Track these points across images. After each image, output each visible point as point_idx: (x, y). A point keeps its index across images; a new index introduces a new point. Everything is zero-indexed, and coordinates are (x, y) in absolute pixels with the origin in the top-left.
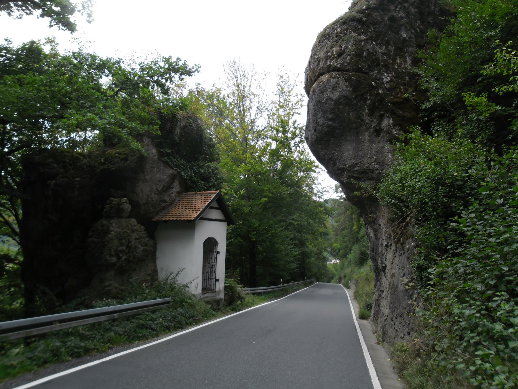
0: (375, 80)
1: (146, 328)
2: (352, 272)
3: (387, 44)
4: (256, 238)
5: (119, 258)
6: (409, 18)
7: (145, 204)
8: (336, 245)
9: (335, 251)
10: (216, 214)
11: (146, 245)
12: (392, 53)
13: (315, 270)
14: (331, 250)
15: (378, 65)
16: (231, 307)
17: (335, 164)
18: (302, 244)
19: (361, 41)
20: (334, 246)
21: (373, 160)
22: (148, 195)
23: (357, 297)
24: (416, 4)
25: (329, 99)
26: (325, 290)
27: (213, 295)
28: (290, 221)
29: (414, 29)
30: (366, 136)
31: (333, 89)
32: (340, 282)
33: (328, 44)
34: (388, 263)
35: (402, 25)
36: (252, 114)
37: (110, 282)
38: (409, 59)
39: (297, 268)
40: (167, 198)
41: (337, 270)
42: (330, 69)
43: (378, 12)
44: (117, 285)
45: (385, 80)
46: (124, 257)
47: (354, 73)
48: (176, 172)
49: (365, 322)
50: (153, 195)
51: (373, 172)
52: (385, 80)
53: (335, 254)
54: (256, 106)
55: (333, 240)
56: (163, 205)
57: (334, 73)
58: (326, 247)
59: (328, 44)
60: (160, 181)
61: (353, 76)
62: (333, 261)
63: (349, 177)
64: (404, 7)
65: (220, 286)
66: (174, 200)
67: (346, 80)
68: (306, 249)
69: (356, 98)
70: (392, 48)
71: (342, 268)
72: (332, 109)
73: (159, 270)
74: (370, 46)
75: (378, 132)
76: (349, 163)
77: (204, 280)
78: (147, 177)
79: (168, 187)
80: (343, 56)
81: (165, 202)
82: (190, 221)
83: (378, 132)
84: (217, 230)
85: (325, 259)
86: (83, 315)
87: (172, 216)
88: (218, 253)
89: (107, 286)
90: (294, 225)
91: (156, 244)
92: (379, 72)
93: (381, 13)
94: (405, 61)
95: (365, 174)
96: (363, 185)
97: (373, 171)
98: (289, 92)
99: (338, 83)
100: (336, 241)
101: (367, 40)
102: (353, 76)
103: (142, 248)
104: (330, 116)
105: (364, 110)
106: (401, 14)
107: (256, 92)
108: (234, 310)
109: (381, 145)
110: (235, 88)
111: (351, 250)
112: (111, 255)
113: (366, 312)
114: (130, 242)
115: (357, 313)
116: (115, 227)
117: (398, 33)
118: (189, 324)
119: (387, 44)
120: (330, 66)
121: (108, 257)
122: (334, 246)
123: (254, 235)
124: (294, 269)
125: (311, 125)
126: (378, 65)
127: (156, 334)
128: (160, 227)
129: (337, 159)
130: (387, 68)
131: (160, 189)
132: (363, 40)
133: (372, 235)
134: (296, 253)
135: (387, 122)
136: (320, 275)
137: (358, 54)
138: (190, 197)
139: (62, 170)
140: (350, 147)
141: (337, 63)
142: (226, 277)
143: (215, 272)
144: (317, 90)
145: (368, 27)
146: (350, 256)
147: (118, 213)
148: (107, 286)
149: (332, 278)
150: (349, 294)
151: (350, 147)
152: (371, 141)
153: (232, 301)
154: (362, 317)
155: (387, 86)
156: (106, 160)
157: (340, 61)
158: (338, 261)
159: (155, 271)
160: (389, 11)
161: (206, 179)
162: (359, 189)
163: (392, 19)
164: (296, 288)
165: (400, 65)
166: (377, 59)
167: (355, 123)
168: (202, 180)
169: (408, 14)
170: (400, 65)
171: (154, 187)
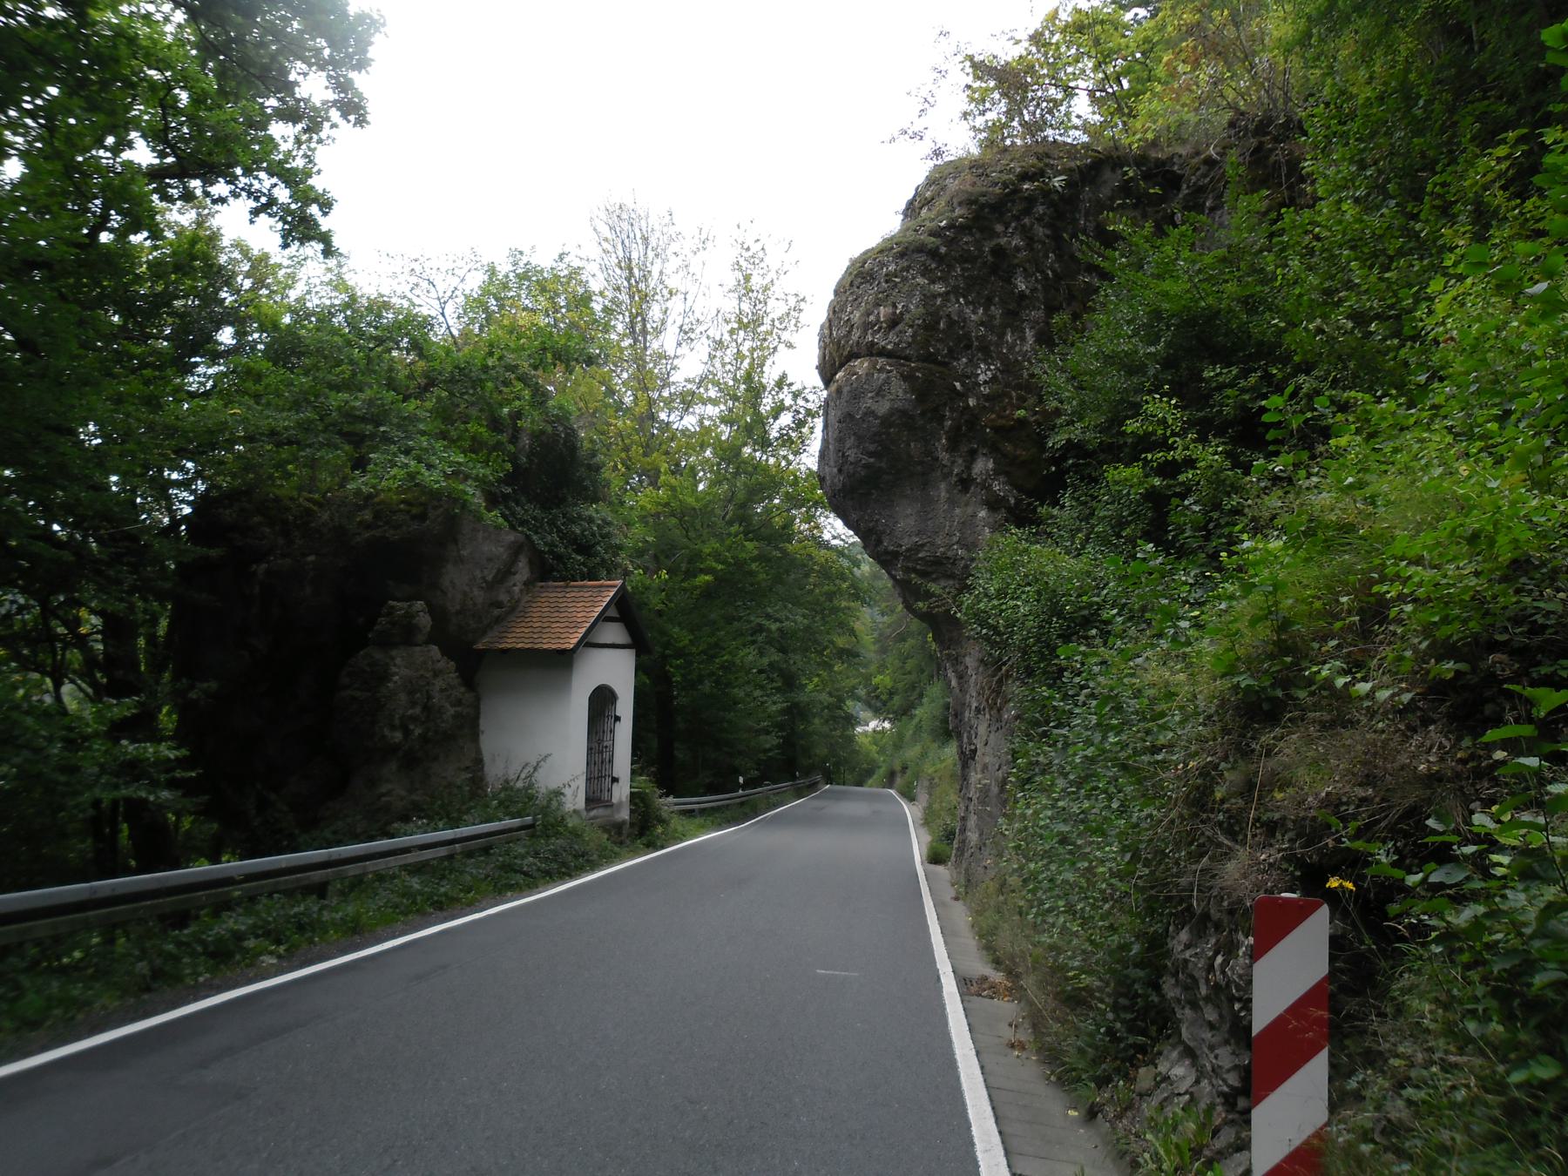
0: (962, 378)
1: (516, 872)
2: (924, 755)
3: (988, 302)
4: (683, 676)
5: (407, 733)
6: (1032, 249)
7: (458, 613)
8: (883, 680)
9: (877, 697)
10: (614, 633)
11: (459, 703)
12: (997, 322)
13: (821, 751)
14: (868, 694)
15: (969, 347)
16: (644, 840)
17: (879, 542)
18: (790, 682)
19: (935, 296)
20: (875, 681)
21: (955, 539)
22: (465, 594)
23: (927, 821)
24: (1047, 219)
25: (870, 413)
26: (853, 804)
27: (607, 812)
28: (758, 620)
29: (1043, 272)
30: (942, 491)
31: (877, 394)
32: (890, 785)
33: (870, 293)
34: (979, 743)
35: (1018, 265)
36: (668, 341)
37: (389, 786)
38: (1029, 334)
39: (778, 746)
40: (504, 597)
41: (882, 751)
42: (872, 351)
43: (972, 235)
44: (403, 793)
45: (982, 378)
46: (418, 731)
47: (920, 364)
48: (521, 538)
49: (940, 868)
50: (476, 592)
51: (954, 564)
52: (982, 378)
53: (879, 706)
54: (679, 323)
55: (873, 668)
56: (496, 612)
57: (881, 361)
58: (854, 688)
59: (870, 293)
60: (490, 560)
61: (918, 369)
62: (873, 724)
63: (907, 570)
64: (1024, 226)
65: (621, 792)
66: (518, 601)
67: (905, 378)
68: (802, 698)
69: (923, 414)
70: (996, 311)
71: (899, 743)
72: (875, 434)
73: (486, 758)
74: (953, 308)
75: (965, 483)
76: (907, 543)
77: (588, 780)
78: (464, 553)
79: (506, 573)
80: (899, 327)
81: (499, 605)
82: (563, 652)
83: (965, 483)
84: (615, 669)
85: (851, 721)
86: (344, 856)
87: (518, 638)
88: (618, 719)
89: (384, 795)
90: (769, 630)
91: (478, 699)
92: (970, 361)
93: (978, 236)
94: (1023, 339)
95: (939, 566)
96: (934, 587)
97: (955, 560)
98: (766, 289)
99: (887, 381)
100: (882, 668)
101: (947, 293)
102: (918, 369)
103: (452, 711)
104: (872, 448)
105: (939, 440)
106: (1017, 241)
107: (672, 283)
108: (652, 846)
109: (970, 510)
110: (619, 275)
111: (921, 696)
112: (393, 728)
113: (943, 847)
114: (429, 698)
115: (925, 851)
116: (402, 666)
117: (1009, 282)
118: (580, 870)
119: (988, 302)
120: (872, 344)
121: (386, 732)
122: (875, 681)
123: (678, 667)
124: (770, 750)
125: (832, 455)
126: (969, 347)
127: (532, 884)
128: (495, 663)
129: (884, 532)
130: (986, 353)
131: (490, 578)
132: (940, 295)
133: (954, 683)
134: (774, 708)
135: (983, 465)
136: (837, 764)
137: (930, 326)
138: (552, 594)
139: (281, 541)
140: (909, 511)
141: (888, 341)
142: (633, 772)
143: (611, 761)
144: (846, 390)
145: (951, 267)
146: (917, 712)
147: (407, 634)
148: (384, 795)
149: (869, 773)
150: (910, 812)
151: (909, 511)
152: (952, 502)
153: (643, 828)
154: (935, 858)
155: (985, 390)
156: (377, 516)
157: (892, 336)
158: (887, 725)
159: (479, 762)
160: (995, 235)
161: (585, 548)
162: (928, 595)
163: (999, 252)
164: (774, 799)
165: (1011, 348)
166: (967, 336)
167: (921, 463)
168: (578, 552)
169: (1030, 240)
170: (1011, 348)
171: (478, 574)
